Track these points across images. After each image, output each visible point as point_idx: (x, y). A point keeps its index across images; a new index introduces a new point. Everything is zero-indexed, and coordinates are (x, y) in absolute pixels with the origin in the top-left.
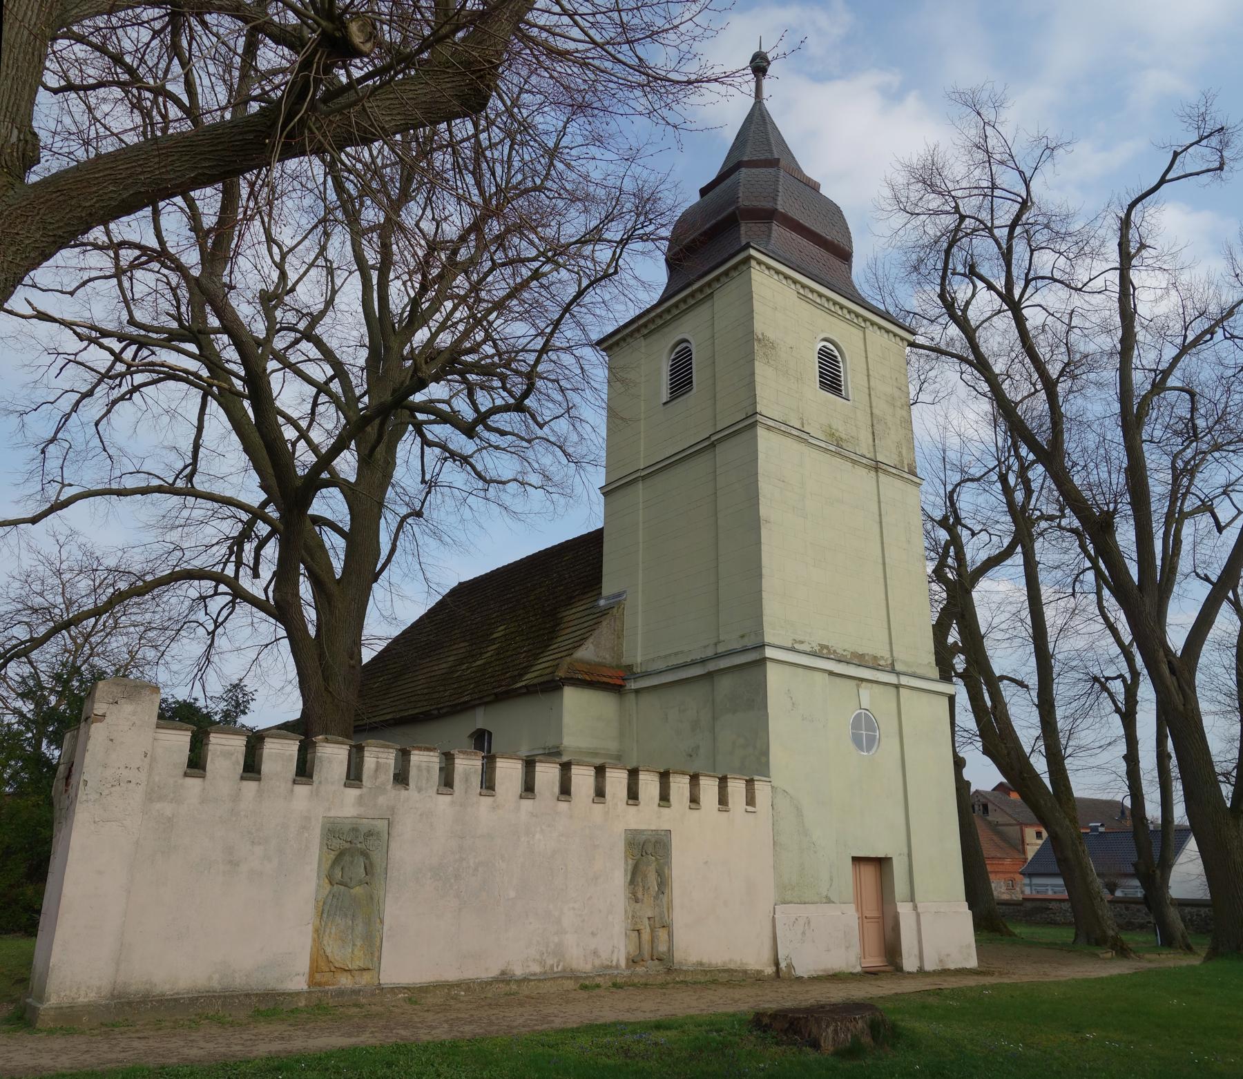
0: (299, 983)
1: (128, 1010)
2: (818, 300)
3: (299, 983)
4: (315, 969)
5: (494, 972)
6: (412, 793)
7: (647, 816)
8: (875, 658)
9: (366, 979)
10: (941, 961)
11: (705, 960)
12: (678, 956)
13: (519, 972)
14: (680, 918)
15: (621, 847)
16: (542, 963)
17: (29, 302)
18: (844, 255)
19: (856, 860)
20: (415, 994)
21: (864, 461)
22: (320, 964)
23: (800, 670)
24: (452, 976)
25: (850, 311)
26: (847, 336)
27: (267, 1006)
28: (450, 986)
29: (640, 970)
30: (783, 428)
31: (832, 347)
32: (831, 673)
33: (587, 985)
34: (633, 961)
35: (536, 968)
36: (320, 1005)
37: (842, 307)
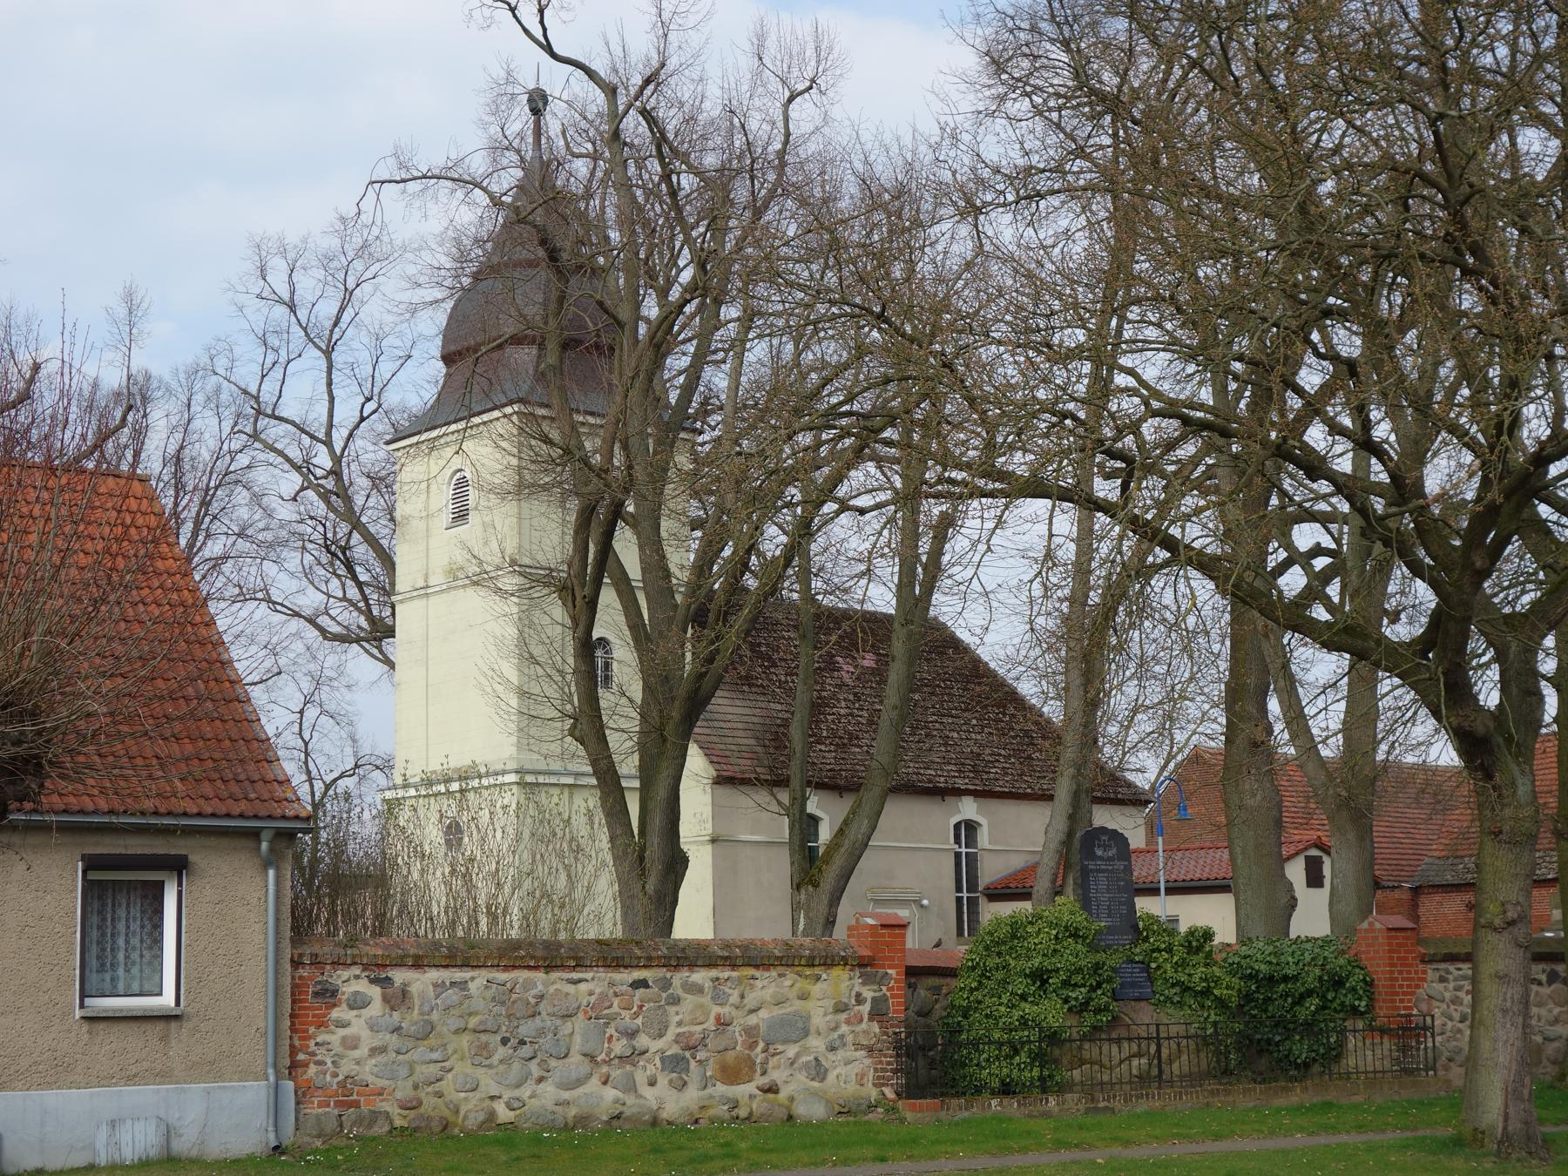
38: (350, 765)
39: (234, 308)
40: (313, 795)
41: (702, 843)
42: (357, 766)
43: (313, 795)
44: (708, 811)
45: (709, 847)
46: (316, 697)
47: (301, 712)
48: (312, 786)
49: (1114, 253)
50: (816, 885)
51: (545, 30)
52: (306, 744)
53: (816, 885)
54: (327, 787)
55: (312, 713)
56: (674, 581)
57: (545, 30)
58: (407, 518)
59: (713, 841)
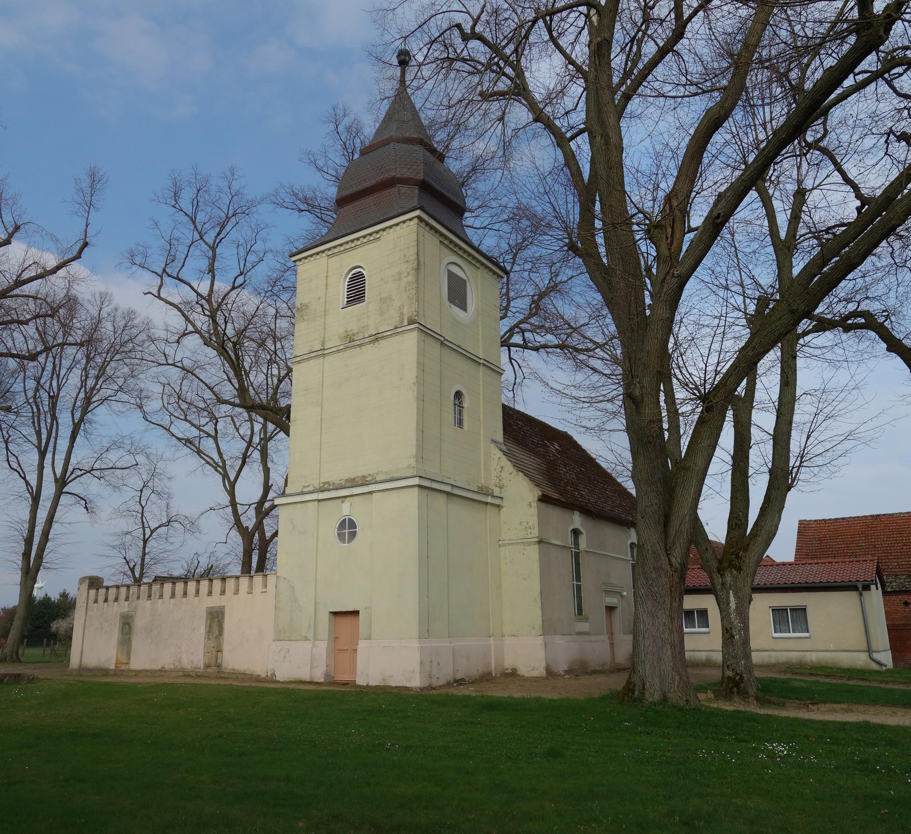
0: (113, 667)
1: (82, 670)
2: (348, 247)
3: (113, 667)
4: (117, 663)
5: (160, 667)
6: (140, 601)
7: (215, 601)
8: (364, 477)
9: (127, 667)
10: (384, 680)
11: (236, 668)
12: (224, 665)
13: (167, 668)
14: (226, 647)
15: (204, 615)
16: (174, 664)
17: (286, 481)
18: (459, 210)
19: (335, 614)
20: (138, 673)
21: (367, 340)
22: (118, 663)
23: (299, 505)
24: (148, 668)
25: (364, 237)
26: (466, 271)
27: (105, 672)
28: (147, 671)
29: (209, 670)
30: (313, 355)
31: (353, 272)
32: (319, 501)
33: (186, 674)
34: (207, 666)
35: (172, 667)
36: (118, 672)
37: (358, 239)
38: (165, 520)
39: (152, 223)
40: (144, 535)
41: (529, 544)
42: (169, 522)
43: (144, 535)
44: (534, 520)
45: (536, 547)
46: (150, 484)
47: (141, 491)
48: (144, 530)
49: (547, 288)
50: (739, 569)
51: (19, 464)
52: (143, 508)
53: (739, 569)
54: (152, 532)
55: (147, 492)
56: (804, 208)
57: (19, 464)
58: (305, 306)
59: (540, 542)
